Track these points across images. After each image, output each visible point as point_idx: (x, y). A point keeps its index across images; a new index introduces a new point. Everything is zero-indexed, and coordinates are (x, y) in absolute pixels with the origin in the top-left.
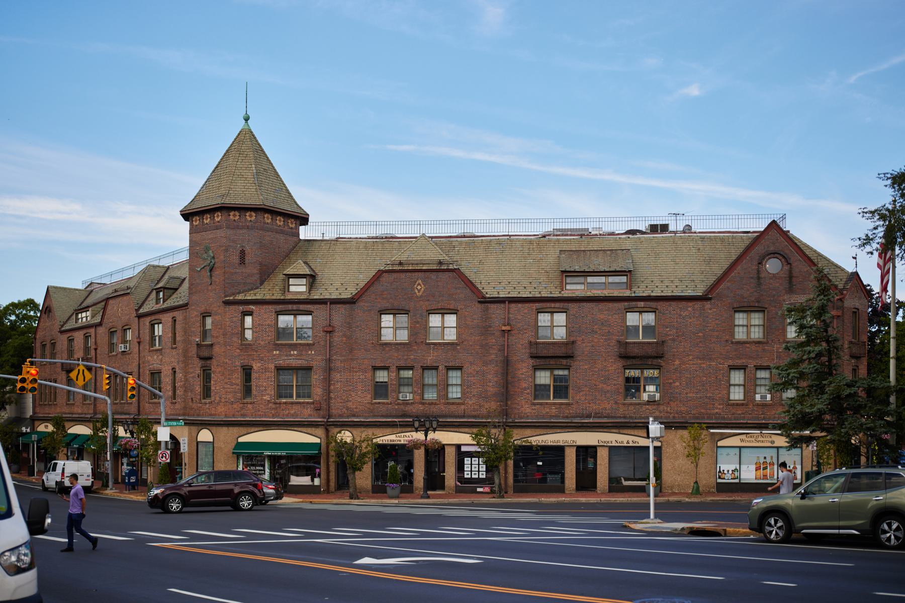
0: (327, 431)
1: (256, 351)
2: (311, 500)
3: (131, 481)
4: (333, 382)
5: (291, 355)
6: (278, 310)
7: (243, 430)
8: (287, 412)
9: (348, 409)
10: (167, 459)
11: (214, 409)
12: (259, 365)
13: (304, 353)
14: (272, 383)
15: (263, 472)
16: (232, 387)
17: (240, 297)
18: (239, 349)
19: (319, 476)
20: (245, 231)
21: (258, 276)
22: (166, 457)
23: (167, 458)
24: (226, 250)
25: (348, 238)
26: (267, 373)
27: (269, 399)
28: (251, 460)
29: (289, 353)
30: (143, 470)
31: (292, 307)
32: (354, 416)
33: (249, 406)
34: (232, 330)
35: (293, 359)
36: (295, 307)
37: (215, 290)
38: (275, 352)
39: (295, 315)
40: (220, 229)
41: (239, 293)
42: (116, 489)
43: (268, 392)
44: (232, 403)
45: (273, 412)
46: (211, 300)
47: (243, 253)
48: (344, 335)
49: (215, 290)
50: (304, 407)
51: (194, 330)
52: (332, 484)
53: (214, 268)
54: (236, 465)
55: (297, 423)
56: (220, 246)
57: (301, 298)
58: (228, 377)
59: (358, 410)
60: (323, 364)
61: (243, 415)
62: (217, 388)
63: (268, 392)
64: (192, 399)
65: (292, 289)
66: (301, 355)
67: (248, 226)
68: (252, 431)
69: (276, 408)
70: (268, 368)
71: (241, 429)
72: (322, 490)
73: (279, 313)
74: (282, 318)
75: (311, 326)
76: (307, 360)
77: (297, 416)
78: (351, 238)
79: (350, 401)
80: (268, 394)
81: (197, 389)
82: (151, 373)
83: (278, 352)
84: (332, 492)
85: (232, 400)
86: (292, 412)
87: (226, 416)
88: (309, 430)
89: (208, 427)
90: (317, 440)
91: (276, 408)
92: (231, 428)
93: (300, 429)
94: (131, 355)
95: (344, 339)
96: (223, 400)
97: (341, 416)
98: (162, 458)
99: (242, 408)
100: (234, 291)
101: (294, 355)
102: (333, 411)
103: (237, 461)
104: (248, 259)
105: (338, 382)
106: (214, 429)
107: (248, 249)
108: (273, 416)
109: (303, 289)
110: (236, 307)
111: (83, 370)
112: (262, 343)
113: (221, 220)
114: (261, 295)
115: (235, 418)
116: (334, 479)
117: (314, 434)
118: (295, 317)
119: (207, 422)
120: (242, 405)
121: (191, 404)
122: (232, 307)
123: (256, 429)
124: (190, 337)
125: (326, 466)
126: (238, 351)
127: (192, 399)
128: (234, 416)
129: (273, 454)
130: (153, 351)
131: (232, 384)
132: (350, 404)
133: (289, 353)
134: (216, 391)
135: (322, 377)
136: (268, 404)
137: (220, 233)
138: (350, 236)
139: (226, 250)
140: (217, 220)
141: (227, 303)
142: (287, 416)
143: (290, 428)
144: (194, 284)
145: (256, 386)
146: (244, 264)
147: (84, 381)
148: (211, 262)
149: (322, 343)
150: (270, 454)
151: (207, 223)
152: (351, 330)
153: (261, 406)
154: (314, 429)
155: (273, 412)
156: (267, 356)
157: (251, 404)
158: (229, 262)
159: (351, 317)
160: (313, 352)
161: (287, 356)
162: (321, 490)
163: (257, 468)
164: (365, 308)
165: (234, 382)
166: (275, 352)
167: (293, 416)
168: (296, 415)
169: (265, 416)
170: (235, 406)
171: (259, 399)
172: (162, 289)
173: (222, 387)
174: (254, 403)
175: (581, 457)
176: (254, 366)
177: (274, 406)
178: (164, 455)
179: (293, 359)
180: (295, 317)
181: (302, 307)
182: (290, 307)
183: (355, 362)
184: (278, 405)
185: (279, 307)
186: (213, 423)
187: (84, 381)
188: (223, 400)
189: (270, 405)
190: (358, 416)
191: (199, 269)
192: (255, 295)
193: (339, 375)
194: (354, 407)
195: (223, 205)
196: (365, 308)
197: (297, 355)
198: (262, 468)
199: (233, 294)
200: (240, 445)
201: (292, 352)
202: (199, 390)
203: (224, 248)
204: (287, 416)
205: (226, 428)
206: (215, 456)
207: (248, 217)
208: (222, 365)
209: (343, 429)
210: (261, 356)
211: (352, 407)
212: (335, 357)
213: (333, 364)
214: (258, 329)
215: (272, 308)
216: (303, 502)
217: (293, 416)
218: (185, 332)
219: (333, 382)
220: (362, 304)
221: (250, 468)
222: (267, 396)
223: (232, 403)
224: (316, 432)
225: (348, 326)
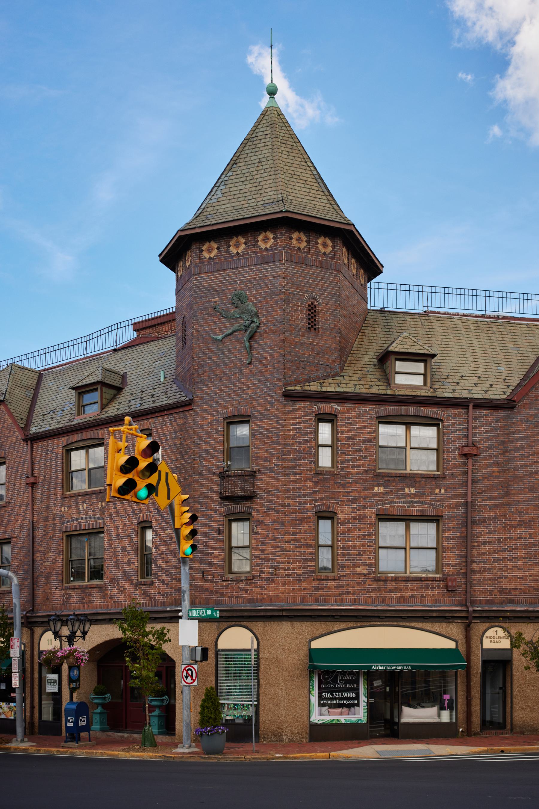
0: (468, 628)
1: (344, 486)
2: (502, 748)
3: (81, 724)
4: (476, 544)
5: (404, 495)
6: (382, 413)
7: (319, 627)
8: (399, 595)
9: (501, 590)
10: (194, 681)
11: (259, 590)
12: (348, 510)
13: (427, 492)
14: (372, 544)
15: (356, 702)
16: (298, 549)
17: (313, 387)
18: (311, 480)
19: (451, 708)
20: (315, 270)
21: (337, 354)
22: (192, 677)
23: (194, 678)
24: (287, 301)
25: (444, 314)
26: (363, 526)
27: (365, 572)
28: (335, 681)
29: (400, 491)
30: (43, 706)
31: (407, 411)
32: (511, 602)
33: (330, 584)
34: (299, 446)
35: (409, 502)
36: (411, 410)
37: (261, 373)
38: (376, 489)
39: (408, 425)
40: (273, 262)
41: (308, 381)
42: (29, 741)
43: (363, 560)
44: (299, 578)
45: (373, 594)
46: (250, 391)
47: (312, 309)
48: (496, 464)
49: (261, 373)
50: (427, 586)
51: (209, 447)
52: (476, 720)
53: (258, 334)
54: (306, 691)
55: (419, 614)
56: (273, 294)
57: (423, 394)
58: (291, 531)
59: (517, 593)
60: (460, 512)
61: (319, 601)
62: (266, 552)
63: (363, 560)
64: (203, 573)
65: (400, 380)
66: (423, 495)
67: (321, 262)
68: (335, 629)
69: (379, 589)
70: (365, 517)
71: (317, 625)
72: (461, 730)
73: (384, 420)
74: (384, 429)
75: (435, 446)
76: (432, 505)
77: (415, 602)
78: (448, 314)
79: (505, 577)
80: (364, 563)
81: (216, 554)
82: (67, 536)
83: (382, 489)
84: (475, 734)
85: (299, 573)
86: (407, 595)
87: (288, 602)
88: (436, 626)
89: (242, 623)
90: (451, 645)
91: (379, 589)
92: (297, 624)
93: (420, 625)
94: (7, 509)
95: (496, 469)
96: (282, 573)
97: (489, 602)
98: (187, 677)
99: (317, 588)
100: (300, 377)
101: (409, 495)
102: (477, 594)
103: (310, 682)
104: (322, 320)
105: (484, 543)
106: (259, 626)
107: (321, 306)
108: (373, 602)
109: (419, 381)
110: (307, 404)
111: (167, 474)
112: (354, 472)
113: (275, 245)
114: (349, 386)
115: (304, 605)
116: (479, 711)
117: (444, 634)
118: (408, 429)
119: (245, 614)
120: (318, 582)
121: (200, 582)
122: (299, 405)
123: (344, 625)
124: (197, 462)
125: (465, 689)
126: (310, 484)
127: (203, 573)
128: (302, 601)
129: (388, 668)
130: (70, 497)
131: (299, 544)
132: (504, 582)
133: (400, 491)
134: (263, 557)
135: (458, 535)
136: (364, 581)
137: (269, 270)
138: (446, 310)
139: (287, 301)
140: (263, 246)
141: (290, 396)
142: (398, 601)
143: (404, 624)
144: (206, 364)
145: (343, 548)
146: (315, 329)
147: (169, 498)
148: (253, 322)
149: (459, 476)
150: (383, 668)
151: (238, 253)
152: (506, 454)
153: (351, 584)
154: (444, 625)
155: (373, 594)
156: (362, 495)
157: (333, 580)
158: (291, 323)
159: (507, 432)
160: (443, 491)
161: (397, 496)
162: (459, 730)
163: (346, 695)
164: (530, 419)
165: (302, 540)
166: (376, 489)
167: (408, 601)
168: (412, 600)
169: (360, 602)
170: (305, 584)
171: (348, 571)
172: (99, 387)
173: (278, 549)
174: (339, 578)
175: (442, 689)
176: (339, 512)
177: (374, 584)
178: (190, 672)
179: (409, 502)
180: (408, 429)
181: (424, 411)
182: (403, 410)
183: (513, 510)
184: (382, 583)
185: (383, 410)
186: (262, 614)
187: (169, 498)
188: (282, 573)
189: (368, 582)
190: (518, 603)
191: (220, 337)
192: (339, 386)
193: (486, 531)
194: (512, 586)
195: (289, 215)
196: (530, 419)
197: (416, 495)
198: (354, 695)
199: (298, 382)
200: (313, 654)
201: (407, 490)
202: (222, 557)
203: (282, 296)
204: (398, 601)
205: (289, 623)
206: (261, 675)
207: (320, 247)
208: (279, 509)
209: (493, 624)
210: (351, 494)
211: (509, 587)
212: (480, 500)
213: (477, 513)
214: (346, 446)
215: (371, 410)
216: (487, 752)
217: (408, 601)
218: (182, 454)
219: (476, 544)
220: (524, 411)
221: (332, 695)
222: (362, 567)
223: (299, 578)
224: (449, 630)
225: (502, 447)
